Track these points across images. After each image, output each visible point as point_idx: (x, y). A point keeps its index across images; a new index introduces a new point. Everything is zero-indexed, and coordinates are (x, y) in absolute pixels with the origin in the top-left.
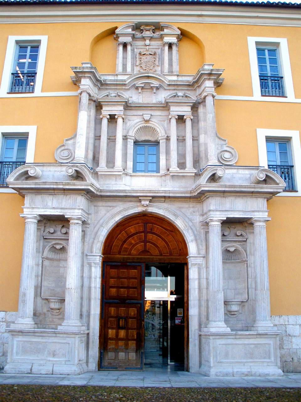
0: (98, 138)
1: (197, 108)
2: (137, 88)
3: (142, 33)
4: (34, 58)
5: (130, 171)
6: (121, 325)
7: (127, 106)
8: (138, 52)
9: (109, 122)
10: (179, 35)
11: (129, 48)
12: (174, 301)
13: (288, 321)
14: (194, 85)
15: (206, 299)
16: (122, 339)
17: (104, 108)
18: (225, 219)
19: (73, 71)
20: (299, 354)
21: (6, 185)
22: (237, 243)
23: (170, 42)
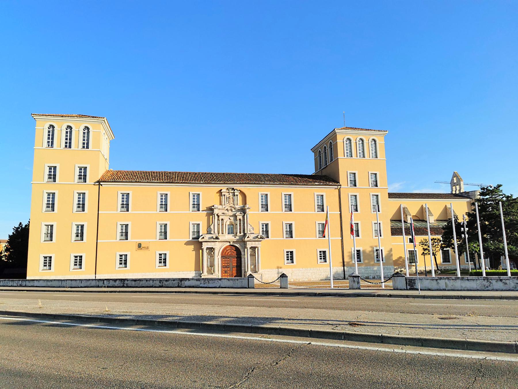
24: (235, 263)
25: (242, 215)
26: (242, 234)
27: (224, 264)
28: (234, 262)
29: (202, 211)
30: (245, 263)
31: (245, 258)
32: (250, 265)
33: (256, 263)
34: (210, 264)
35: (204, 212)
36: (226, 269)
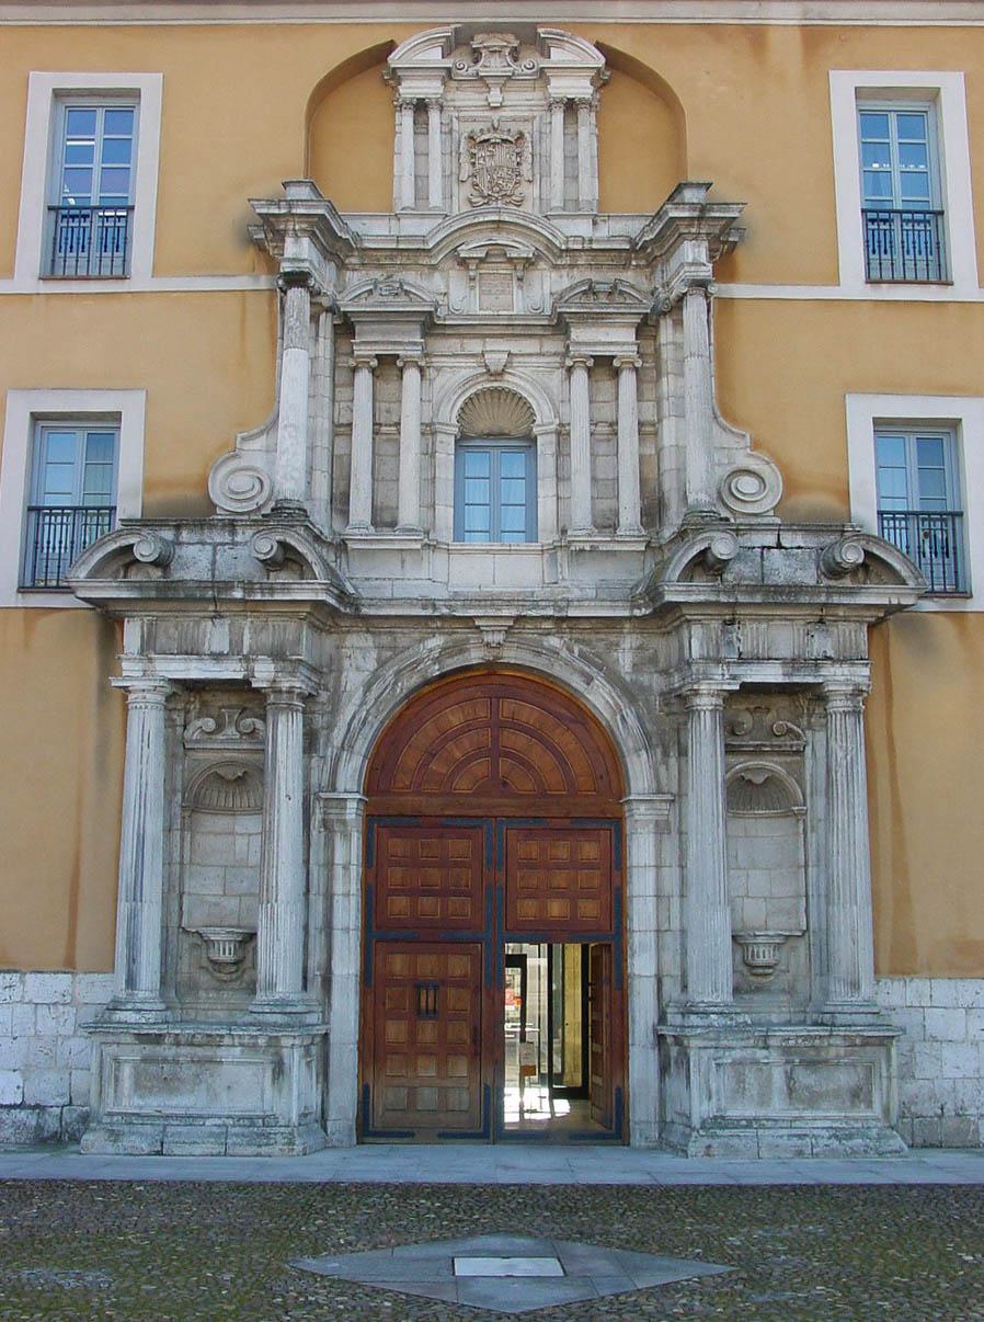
1: (657, 327)
2: (463, 262)
4: (121, 150)
5: (444, 533)
6: (423, 1004)
7: (430, 325)
8: (466, 135)
9: (378, 377)
10: (599, 69)
11: (434, 117)
12: (579, 1088)
13: (931, 996)
14: (649, 253)
15: (679, 927)
20: (960, 1096)
21: (42, 584)
22: (776, 759)
23: (569, 96)
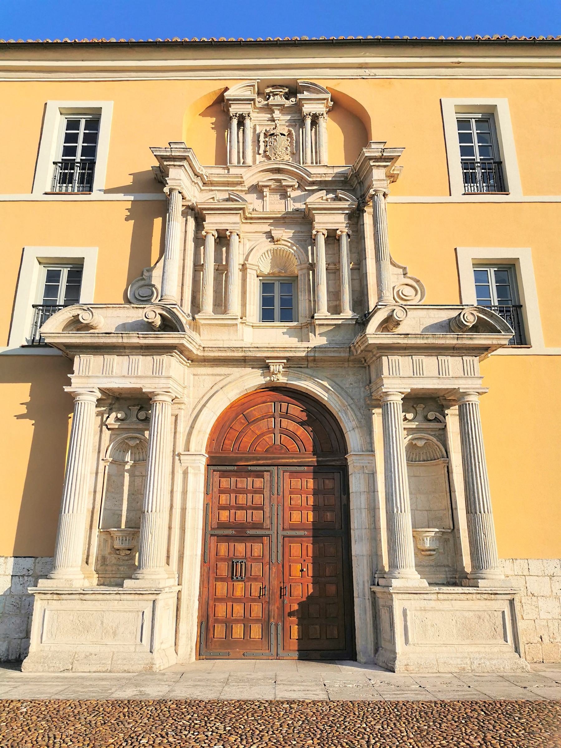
0: (198, 267)
3: (268, 99)
16: (237, 621)
17: (209, 219)
18: (409, 391)
19: (155, 155)
24: (300, 509)
25: (345, 205)
26: (348, 313)
27: (224, 515)
28: (297, 499)
29: (106, 191)
30: (373, 510)
31: (373, 474)
32: (414, 526)
33: (453, 509)
34: (128, 510)
35: (121, 196)
36: (240, 547)
